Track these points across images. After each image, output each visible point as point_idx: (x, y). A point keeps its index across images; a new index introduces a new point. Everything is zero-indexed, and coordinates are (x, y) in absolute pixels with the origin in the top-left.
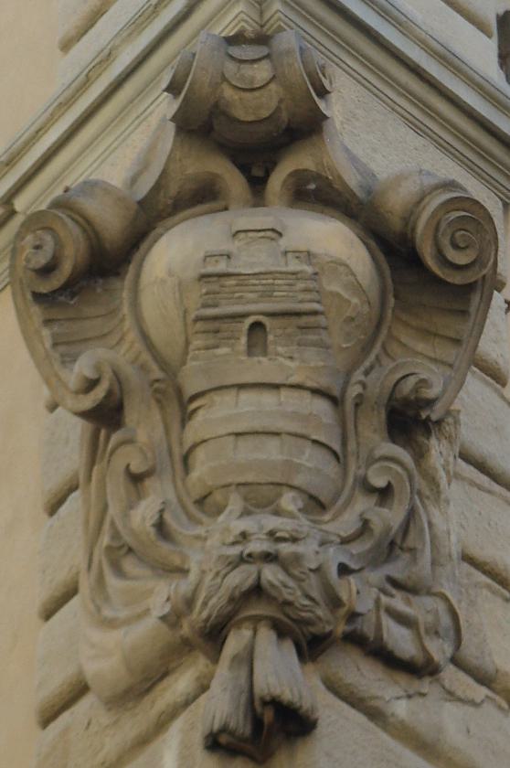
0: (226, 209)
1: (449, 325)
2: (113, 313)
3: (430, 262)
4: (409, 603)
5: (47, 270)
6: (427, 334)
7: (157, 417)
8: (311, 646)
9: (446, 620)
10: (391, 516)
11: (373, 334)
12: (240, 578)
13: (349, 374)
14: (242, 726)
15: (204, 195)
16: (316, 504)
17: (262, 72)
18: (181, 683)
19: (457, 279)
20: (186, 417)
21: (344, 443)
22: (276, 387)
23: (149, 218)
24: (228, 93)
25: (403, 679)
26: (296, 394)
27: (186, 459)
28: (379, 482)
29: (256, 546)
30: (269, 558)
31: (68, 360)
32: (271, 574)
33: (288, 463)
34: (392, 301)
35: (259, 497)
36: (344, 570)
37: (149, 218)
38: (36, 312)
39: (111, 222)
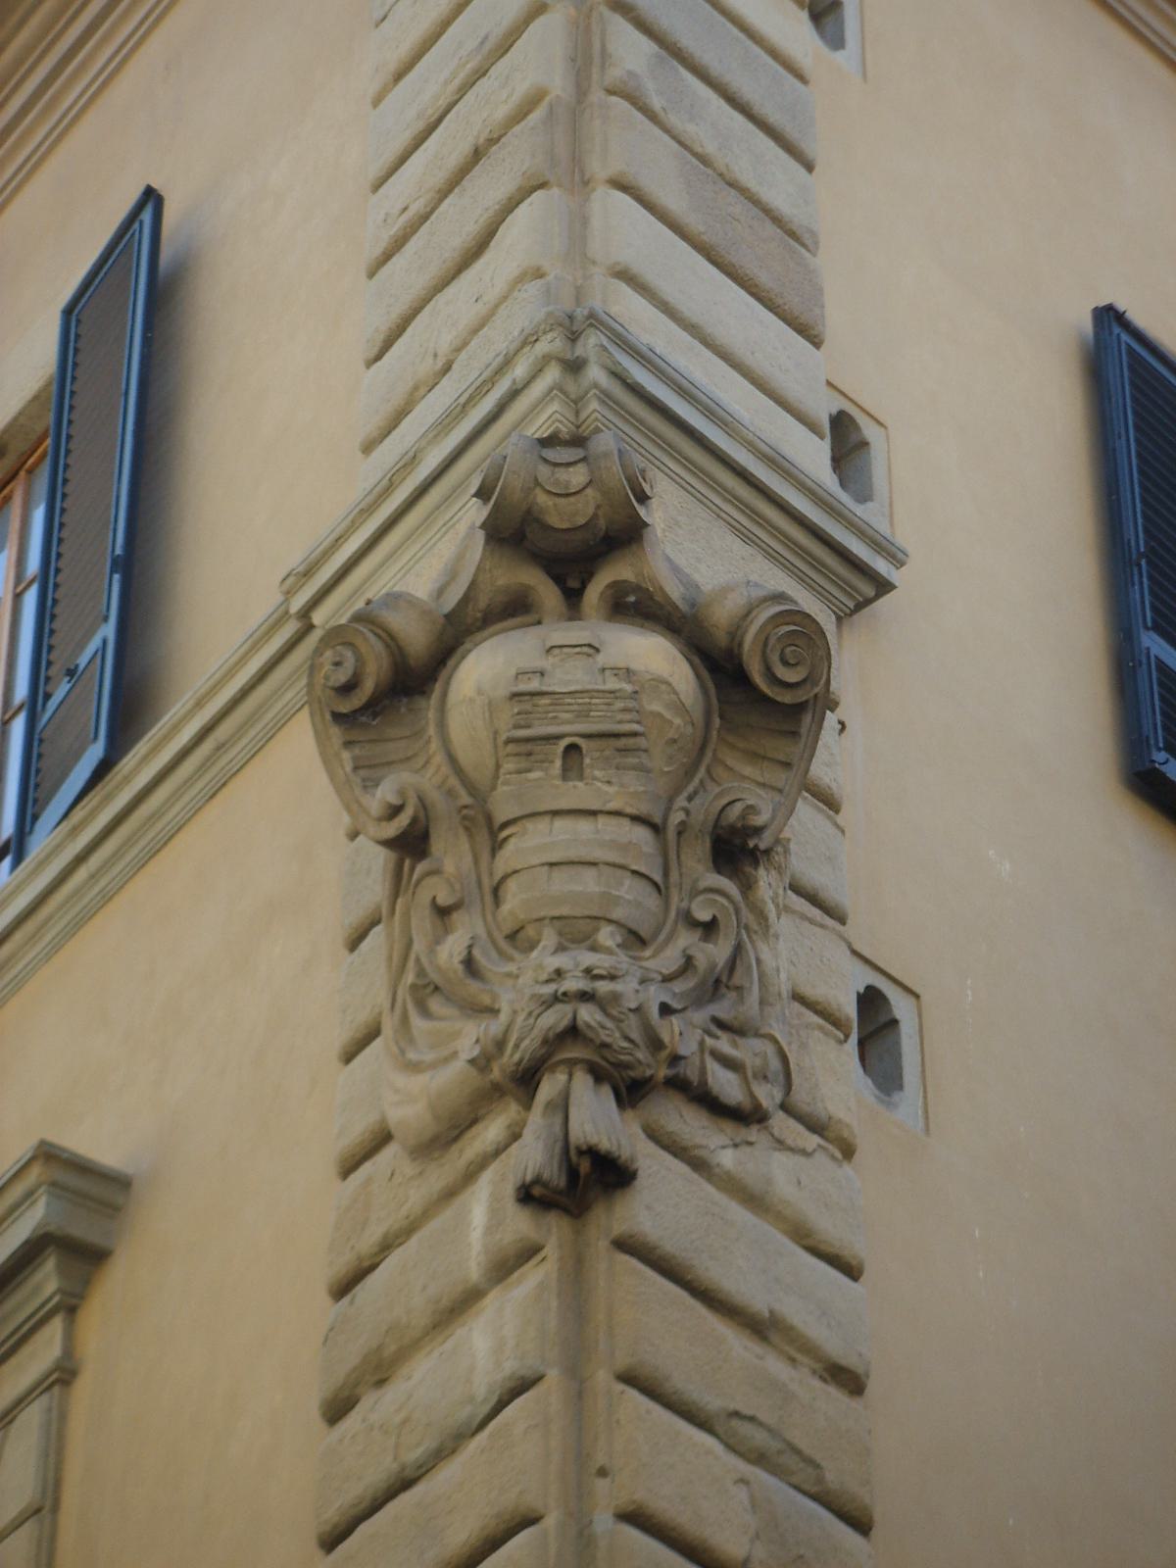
0: (539, 623)
2: (418, 734)
4: (735, 1045)
5: (347, 689)
6: (755, 757)
8: (630, 1091)
9: (775, 1064)
10: (717, 952)
11: (696, 757)
12: (555, 1019)
13: (671, 800)
14: (559, 1180)
15: (516, 608)
16: (635, 940)
17: (577, 476)
18: (491, 1131)
19: (786, 698)
20: (496, 846)
21: (666, 874)
23: (457, 632)
24: (542, 499)
26: (614, 821)
27: (496, 891)
28: (704, 915)
29: (572, 984)
30: (585, 996)
31: (368, 771)
32: (587, 1014)
34: (717, 722)
35: (575, 932)
37: (457, 632)
38: (336, 733)
39: (416, 636)
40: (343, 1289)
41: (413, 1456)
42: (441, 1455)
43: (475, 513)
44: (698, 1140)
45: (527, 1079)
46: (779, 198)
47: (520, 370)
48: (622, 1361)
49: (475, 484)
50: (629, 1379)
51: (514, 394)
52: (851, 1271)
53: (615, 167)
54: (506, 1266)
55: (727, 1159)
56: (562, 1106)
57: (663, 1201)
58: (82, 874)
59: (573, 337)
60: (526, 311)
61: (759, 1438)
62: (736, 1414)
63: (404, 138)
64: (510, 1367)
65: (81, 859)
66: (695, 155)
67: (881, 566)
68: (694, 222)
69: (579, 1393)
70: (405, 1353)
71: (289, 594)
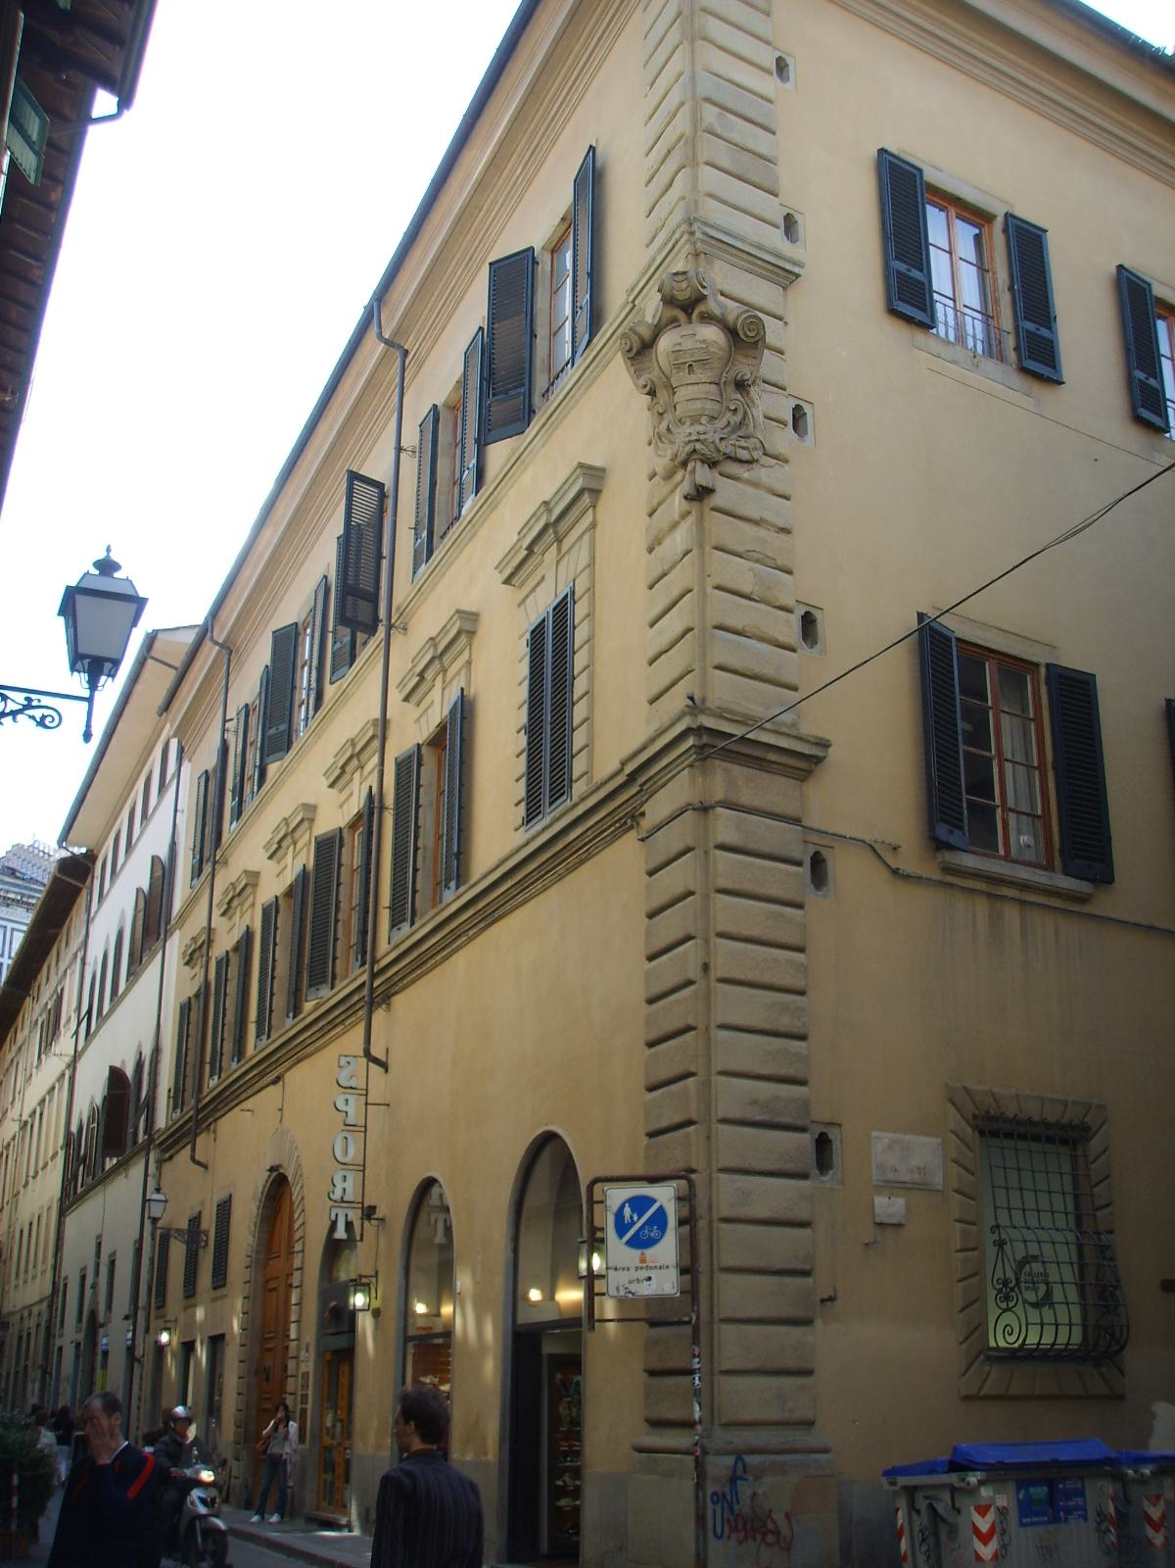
0: (680, 326)
1: (751, 352)
2: (651, 360)
3: (741, 333)
4: (746, 442)
5: (630, 350)
6: (746, 356)
7: (666, 394)
8: (713, 464)
9: (759, 445)
10: (739, 417)
11: (729, 359)
12: (689, 448)
13: (721, 374)
14: (694, 493)
15: (673, 322)
16: (713, 418)
17: (684, 285)
18: (679, 476)
19: (752, 340)
20: (674, 393)
21: (722, 398)
22: (698, 383)
23: (658, 331)
24: (675, 292)
25: (746, 465)
26: (559, 568)
27: (675, 407)
28: (733, 408)
29: (693, 438)
30: (697, 440)
31: (639, 377)
32: (698, 446)
33: (702, 408)
34: (733, 349)
35: (695, 420)
36: (721, 439)
37: (658, 331)
38: (629, 362)
39: (646, 333)
40: (651, 515)
41: (666, 567)
42: (673, 567)
43: (659, 296)
44: (736, 472)
45: (684, 464)
46: (762, 150)
47: (677, 235)
48: (714, 544)
49: (656, 288)
50: (716, 548)
51: (677, 242)
52: (787, 498)
53: (705, 158)
54: (685, 515)
55: (746, 475)
56: (693, 471)
57: (727, 492)
58: (588, 372)
59: (691, 225)
60: (678, 217)
61: (757, 556)
62: (749, 551)
63: (651, 142)
64: (685, 547)
65: (587, 367)
66: (733, 144)
67: (796, 270)
68: (733, 169)
69: (702, 554)
70: (663, 537)
71: (628, 295)
